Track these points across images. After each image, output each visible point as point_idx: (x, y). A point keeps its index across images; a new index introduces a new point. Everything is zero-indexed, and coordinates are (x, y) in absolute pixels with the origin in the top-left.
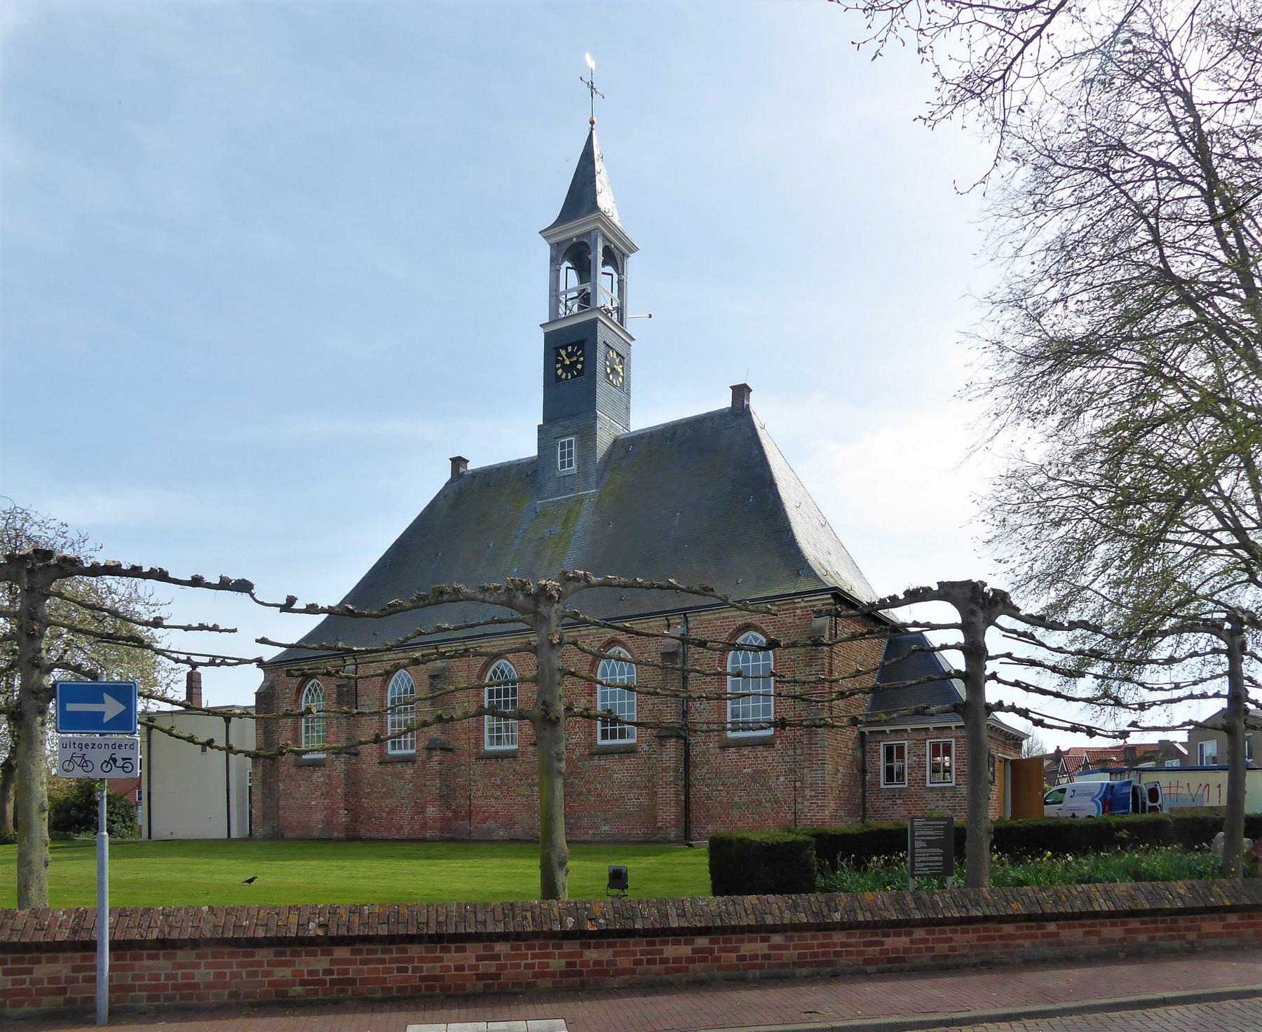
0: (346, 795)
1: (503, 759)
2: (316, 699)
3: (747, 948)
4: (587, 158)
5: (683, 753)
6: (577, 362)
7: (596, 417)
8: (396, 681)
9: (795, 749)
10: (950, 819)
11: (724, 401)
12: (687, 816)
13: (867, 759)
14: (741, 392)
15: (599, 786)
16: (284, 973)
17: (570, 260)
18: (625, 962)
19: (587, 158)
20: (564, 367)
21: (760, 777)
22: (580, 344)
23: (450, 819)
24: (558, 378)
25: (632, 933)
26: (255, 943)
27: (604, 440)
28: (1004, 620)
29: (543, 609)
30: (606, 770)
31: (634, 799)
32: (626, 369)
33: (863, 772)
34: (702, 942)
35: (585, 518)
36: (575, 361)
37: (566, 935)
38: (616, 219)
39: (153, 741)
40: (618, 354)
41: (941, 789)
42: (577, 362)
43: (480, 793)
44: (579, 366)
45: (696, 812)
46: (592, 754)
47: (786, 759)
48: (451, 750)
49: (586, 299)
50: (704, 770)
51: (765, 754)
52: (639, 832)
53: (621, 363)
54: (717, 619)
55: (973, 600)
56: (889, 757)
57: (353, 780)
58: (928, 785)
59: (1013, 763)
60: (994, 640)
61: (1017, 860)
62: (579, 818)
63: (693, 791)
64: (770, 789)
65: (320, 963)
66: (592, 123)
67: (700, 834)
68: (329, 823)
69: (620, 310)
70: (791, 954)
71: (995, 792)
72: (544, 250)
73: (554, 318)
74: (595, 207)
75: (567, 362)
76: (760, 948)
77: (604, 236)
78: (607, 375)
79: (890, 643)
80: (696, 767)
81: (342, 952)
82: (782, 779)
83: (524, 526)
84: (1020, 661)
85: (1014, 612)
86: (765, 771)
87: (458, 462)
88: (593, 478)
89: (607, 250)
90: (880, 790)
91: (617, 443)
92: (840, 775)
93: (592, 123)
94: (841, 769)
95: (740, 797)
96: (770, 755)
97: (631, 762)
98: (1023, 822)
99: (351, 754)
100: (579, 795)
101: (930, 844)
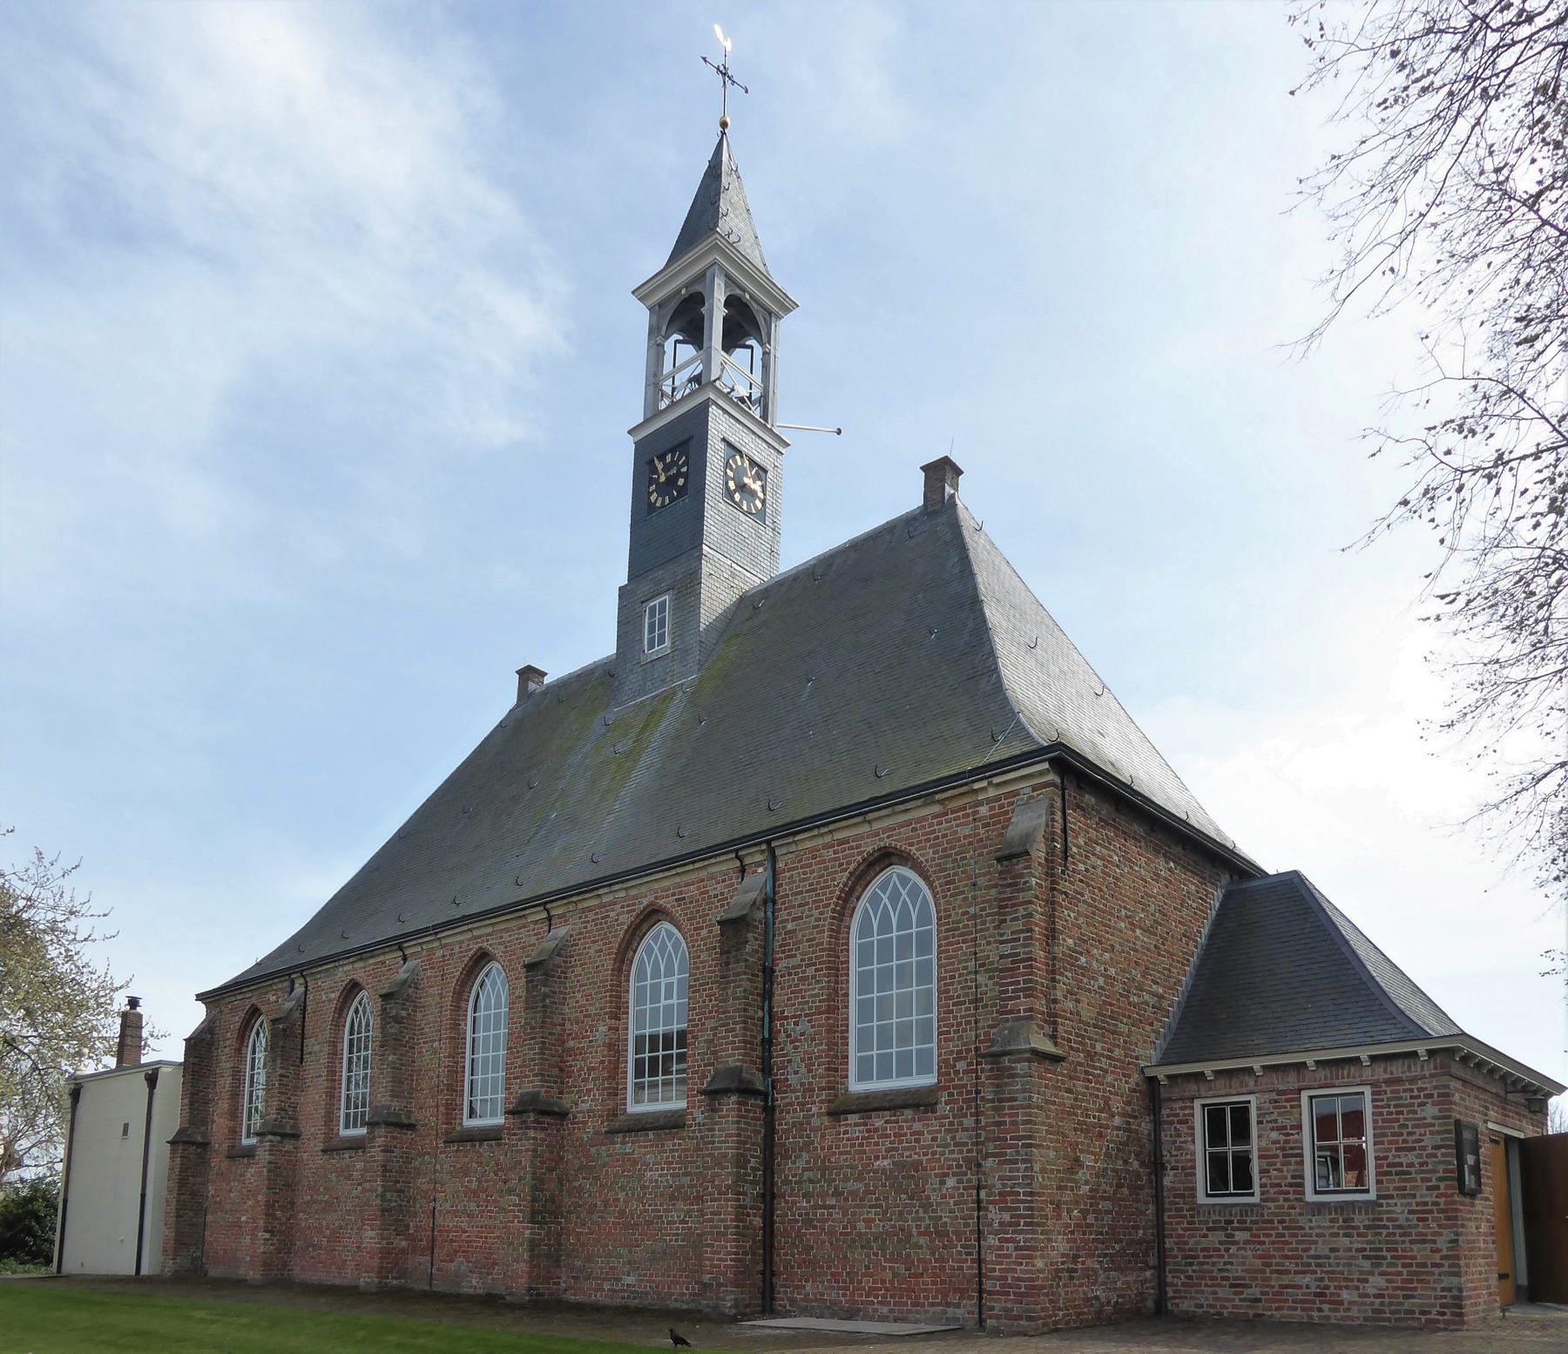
1: (481, 1141)
4: (714, 172)
5: (760, 1126)
6: (679, 475)
8: (357, 1011)
9: (977, 1114)
11: (910, 497)
12: (768, 1259)
13: (1166, 1137)
14: (941, 473)
15: (621, 1195)
17: (681, 331)
21: (907, 1176)
23: (403, 1251)
24: (651, 507)
30: (635, 1163)
33: (1157, 1166)
39: (77, 1127)
40: (753, 463)
41: (1341, 1207)
42: (679, 475)
43: (447, 1206)
44: (681, 482)
45: (786, 1254)
46: (612, 1132)
47: (961, 1136)
48: (411, 1127)
50: (801, 1164)
51: (917, 1126)
53: (758, 477)
54: (827, 847)
56: (1216, 1134)
58: (1310, 1197)
59: (1523, 1144)
62: (589, 1258)
63: (780, 1207)
64: (927, 1206)
66: (724, 125)
67: (793, 1301)
69: (764, 401)
72: (641, 316)
73: (652, 414)
75: (663, 479)
77: (728, 276)
78: (729, 494)
79: (1228, 896)
80: (786, 1157)
82: (951, 1182)
86: (917, 1165)
90: (1196, 1208)
91: (749, 605)
92: (1081, 1175)
93: (724, 125)
94: (1088, 1160)
95: (868, 1222)
96: (928, 1129)
99: (284, 1135)
100: (590, 1212)
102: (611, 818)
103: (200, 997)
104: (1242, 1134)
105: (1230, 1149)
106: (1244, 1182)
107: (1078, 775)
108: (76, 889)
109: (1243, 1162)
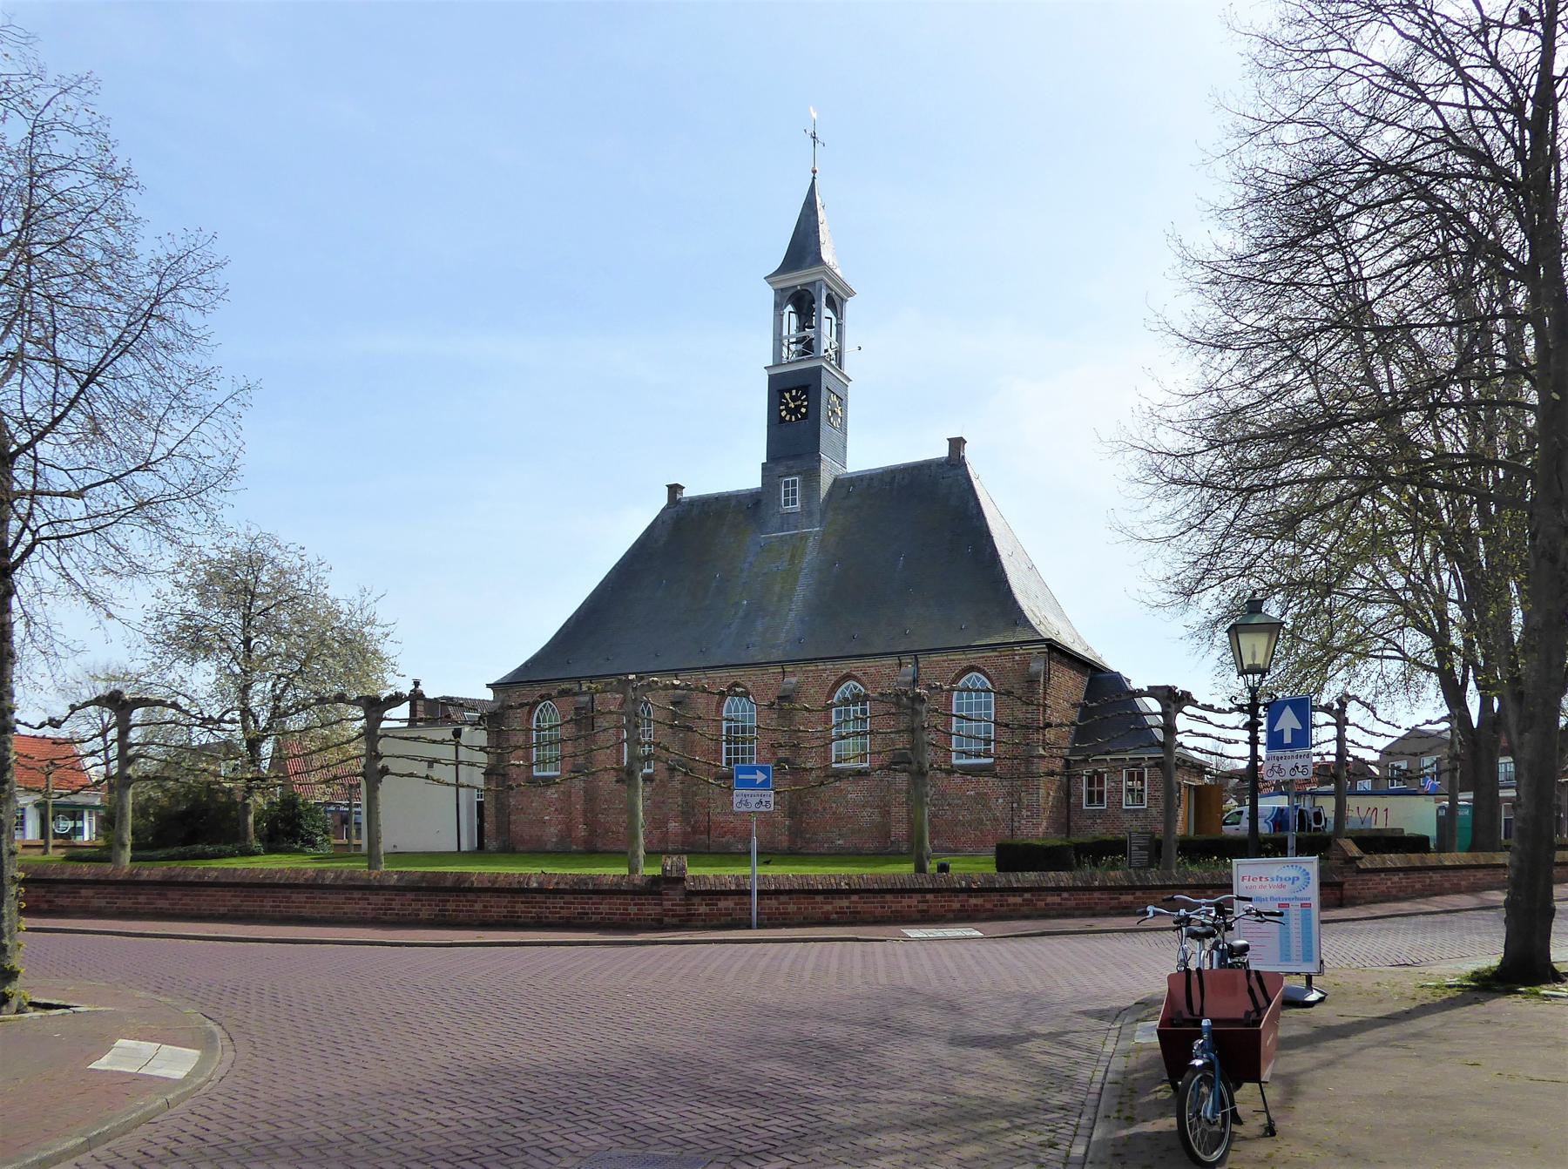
0: (585, 811)
2: (550, 716)
3: (1050, 899)
4: (810, 206)
7: (819, 460)
10: (1153, 834)
11: (943, 452)
14: (957, 444)
16: (828, 908)
17: (794, 305)
18: (989, 906)
19: (810, 206)
20: (788, 410)
21: (982, 798)
22: (805, 389)
24: (782, 419)
25: (995, 890)
26: (817, 892)
27: (826, 481)
28: (1188, 709)
29: (917, 707)
31: (868, 816)
32: (844, 411)
33: (1068, 795)
34: (1027, 896)
35: (811, 555)
36: (800, 405)
37: (962, 890)
38: (838, 271)
49: (808, 347)
52: (870, 846)
55: (1169, 698)
56: (1091, 783)
57: (590, 797)
60: (1181, 722)
61: (1193, 862)
65: (845, 903)
68: (567, 833)
70: (1072, 903)
71: (1181, 813)
72: (769, 295)
74: (819, 260)
76: (1057, 899)
81: (855, 898)
83: (750, 559)
84: (1198, 735)
85: (1194, 703)
87: (674, 489)
88: (818, 517)
89: (829, 297)
97: (864, 783)
98: (1204, 836)
101: (1141, 848)
102: (792, 614)
103: (488, 686)
104: (1101, 783)
105: (1096, 788)
106: (1101, 801)
107: (1058, 652)
108: (383, 614)
109: (1101, 794)
